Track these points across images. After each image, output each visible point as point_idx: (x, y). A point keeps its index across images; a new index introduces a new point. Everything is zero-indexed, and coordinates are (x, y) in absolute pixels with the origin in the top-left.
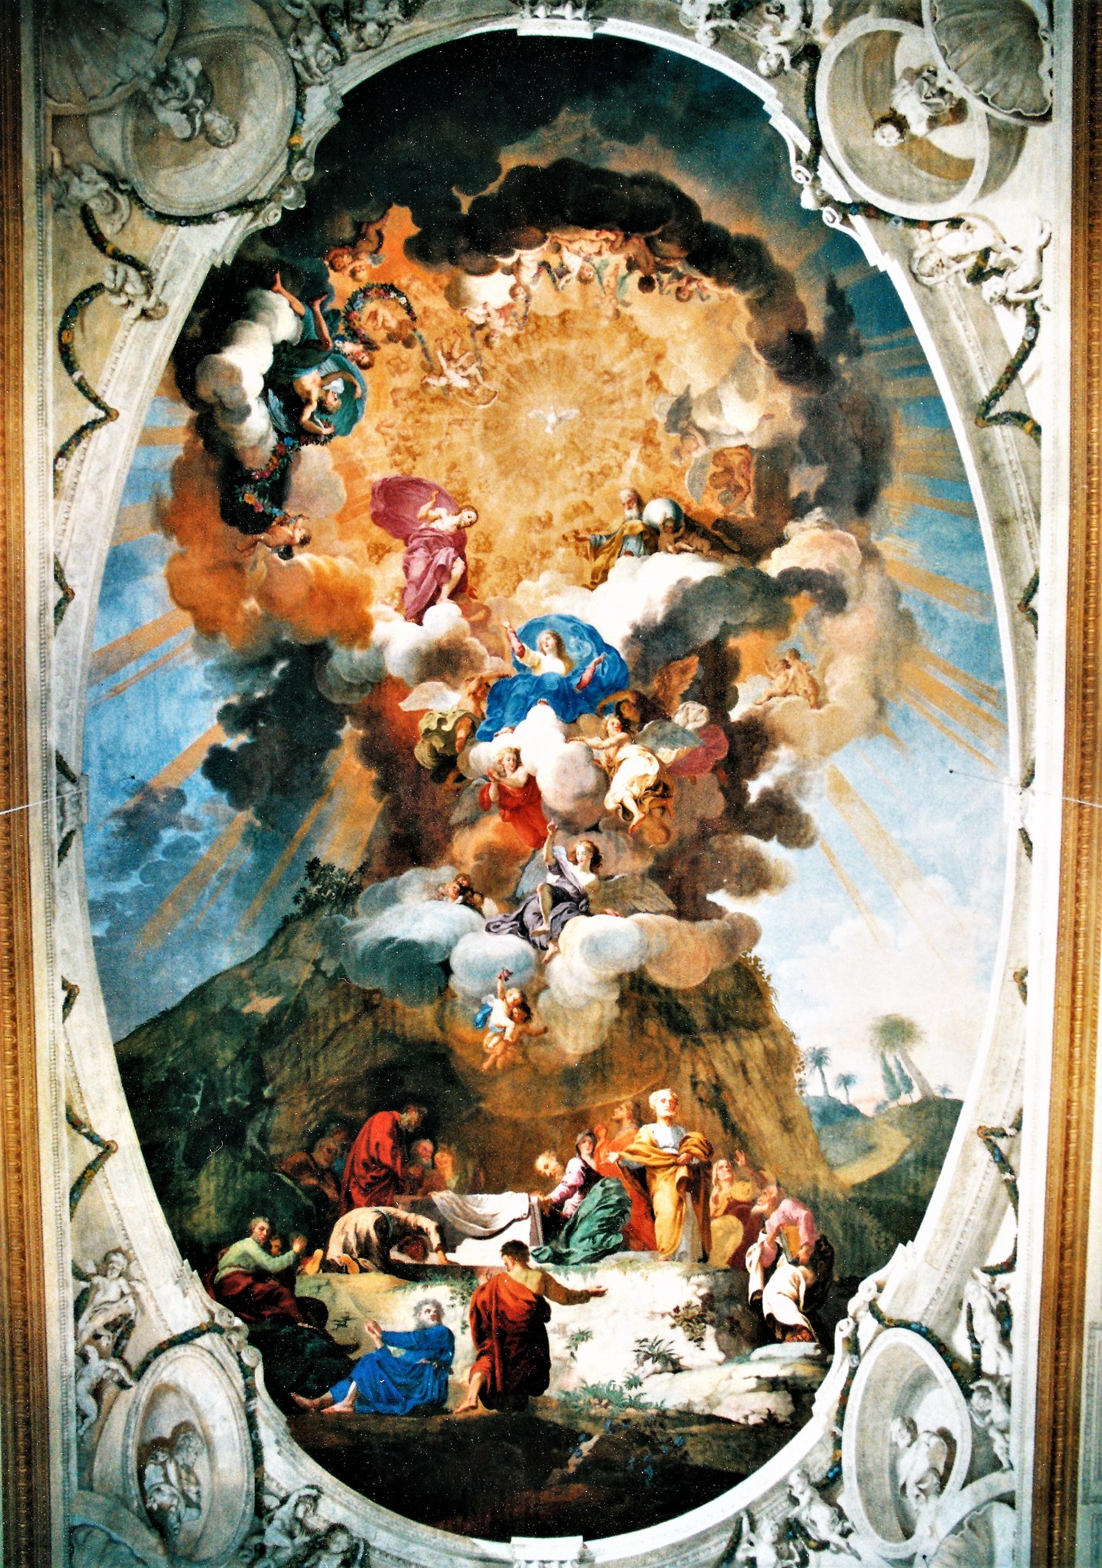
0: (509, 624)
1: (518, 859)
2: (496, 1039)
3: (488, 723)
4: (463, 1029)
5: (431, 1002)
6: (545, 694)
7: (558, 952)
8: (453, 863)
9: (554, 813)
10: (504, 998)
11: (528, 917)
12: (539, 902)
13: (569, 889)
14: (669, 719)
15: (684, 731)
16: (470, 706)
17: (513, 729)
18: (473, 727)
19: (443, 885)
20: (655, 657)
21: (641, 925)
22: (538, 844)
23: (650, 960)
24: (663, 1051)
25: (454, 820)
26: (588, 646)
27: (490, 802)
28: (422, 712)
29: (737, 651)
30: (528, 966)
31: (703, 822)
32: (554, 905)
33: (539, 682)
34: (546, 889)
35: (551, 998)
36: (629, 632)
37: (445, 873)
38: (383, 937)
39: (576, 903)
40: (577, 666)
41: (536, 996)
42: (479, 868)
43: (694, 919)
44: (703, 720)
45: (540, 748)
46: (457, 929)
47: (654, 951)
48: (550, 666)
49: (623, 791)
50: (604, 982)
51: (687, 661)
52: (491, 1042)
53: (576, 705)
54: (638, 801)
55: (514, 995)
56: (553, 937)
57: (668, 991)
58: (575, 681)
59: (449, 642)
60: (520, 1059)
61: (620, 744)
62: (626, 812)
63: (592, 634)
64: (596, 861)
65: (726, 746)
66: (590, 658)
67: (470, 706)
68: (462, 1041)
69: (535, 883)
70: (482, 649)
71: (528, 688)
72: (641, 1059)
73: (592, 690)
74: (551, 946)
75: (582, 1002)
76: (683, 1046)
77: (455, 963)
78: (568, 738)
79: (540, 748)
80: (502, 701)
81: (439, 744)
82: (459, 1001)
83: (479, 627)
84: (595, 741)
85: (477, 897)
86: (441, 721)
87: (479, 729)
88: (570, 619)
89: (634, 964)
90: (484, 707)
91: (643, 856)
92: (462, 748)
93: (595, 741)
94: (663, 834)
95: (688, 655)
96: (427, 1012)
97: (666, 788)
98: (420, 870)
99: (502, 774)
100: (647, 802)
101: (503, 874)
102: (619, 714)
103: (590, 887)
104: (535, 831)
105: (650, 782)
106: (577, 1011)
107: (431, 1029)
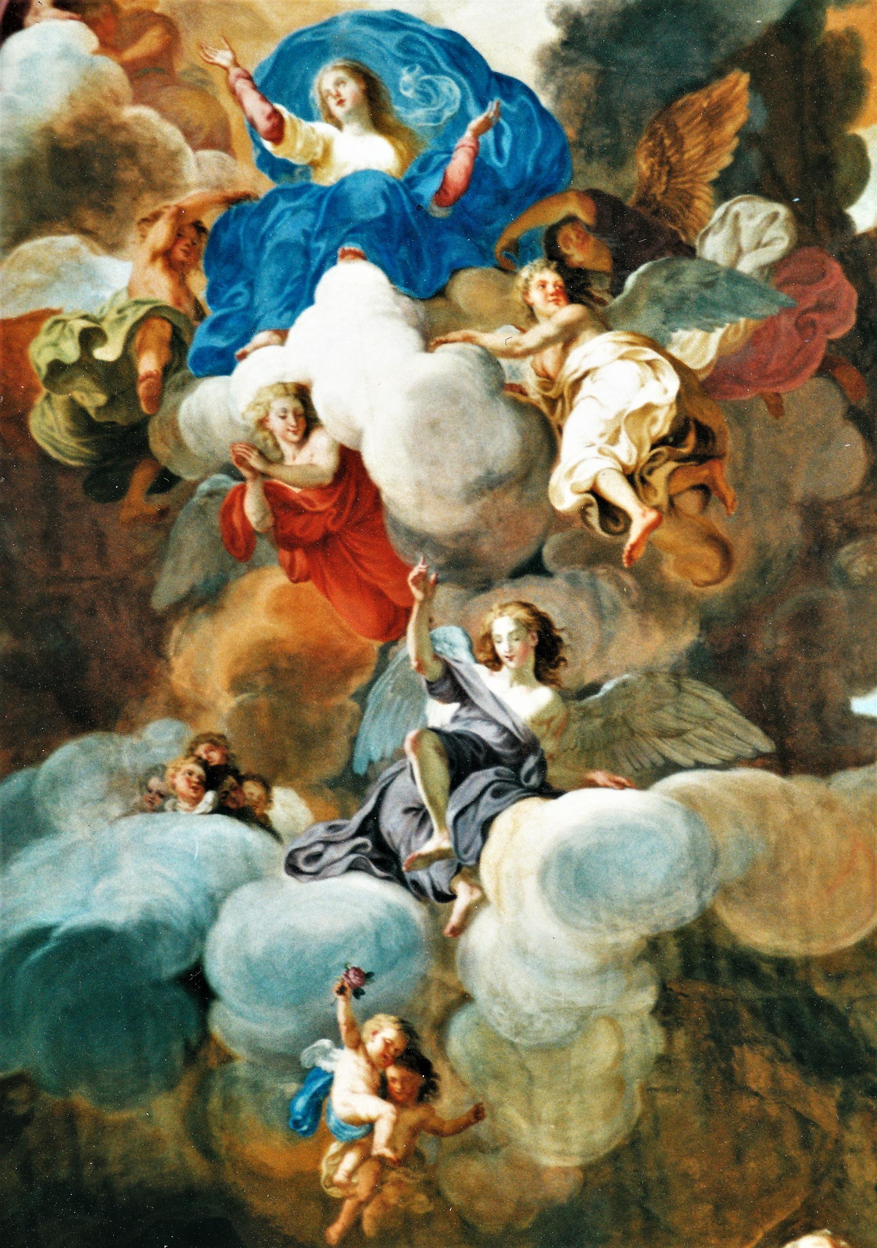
0: (232, 55)
1: (348, 672)
2: (351, 1159)
3: (216, 327)
4: (266, 1147)
5: (171, 1086)
6: (355, 232)
7: (483, 900)
8: (178, 708)
9: (422, 540)
10: (358, 1044)
11: (393, 823)
12: (418, 778)
13: (488, 734)
14: (690, 252)
15: (733, 276)
16: (160, 288)
17: (282, 334)
18: (177, 343)
19: (158, 770)
20: (633, 92)
21: (690, 803)
22: (392, 627)
23: (725, 891)
24: (791, 1134)
25: (161, 600)
26: (451, 88)
27: (250, 534)
28: (35, 319)
29: (851, 40)
30: (409, 949)
31: (813, 511)
32: (455, 782)
33: (335, 200)
34: (430, 743)
35: (480, 1023)
36: (553, 34)
37: (160, 741)
38: (18, 928)
39: (520, 768)
40: (429, 145)
41: (441, 1026)
42: (245, 712)
43: (825, 767)
44: (780, 240)
45: (358, 367)
46: (213, 880)
47: (732, 869)
48: (359, 154)
49: (589, 459)
50: (615, 964)
51: (719, 89)
52: (341, 1167)
53: (439, 249)
54: (636, 478)
55: (383, 1033)
56: (465, 865)
57: (784, 966)
58: (428, 188)
59: (78, 125)
60: (421, 1204)
61: (568, 337)
62: (610, 512)
63: (459, 53)
64: (547, 652)
65: (849, 296)
66: (461, 120)
67: (160, 288)
68: (259, 1175)
69: (403, 733)
70: (171, 135)
71: (307, 220)
72: (739, 1156)
73: (479, 202)
74: (462, 890)
75: (563, 1025)
76: (845, 1109)
77: (219, 970)
78: (430, 337)
79: (358, 367)
80: (243, 267)
81: (92, 399)
82: (241, 1068)
83: (151, 75)
84: (498, 338)
85: (252, 790)
86: (90, 337)
87: (197, 347)
88: (394, 22)
89: (685, 906)
90: (199, 284)
91: (667, 623)
92: (156, 401)
93: (498, 338)
94: (711, 556)
95: (720, 73)
96: (162, 1114)
97: (705, 434)
98: (90, 739)
99: (271, 456)
100: (658, 478)
101: (312, 718)
102: (555, 257)
103: (538, 721)
104: (378, 595)
105: (661, 426)
106: (553, 1050)
107: (177, 1154)
